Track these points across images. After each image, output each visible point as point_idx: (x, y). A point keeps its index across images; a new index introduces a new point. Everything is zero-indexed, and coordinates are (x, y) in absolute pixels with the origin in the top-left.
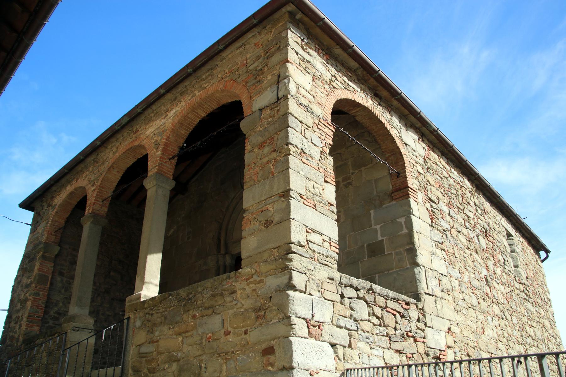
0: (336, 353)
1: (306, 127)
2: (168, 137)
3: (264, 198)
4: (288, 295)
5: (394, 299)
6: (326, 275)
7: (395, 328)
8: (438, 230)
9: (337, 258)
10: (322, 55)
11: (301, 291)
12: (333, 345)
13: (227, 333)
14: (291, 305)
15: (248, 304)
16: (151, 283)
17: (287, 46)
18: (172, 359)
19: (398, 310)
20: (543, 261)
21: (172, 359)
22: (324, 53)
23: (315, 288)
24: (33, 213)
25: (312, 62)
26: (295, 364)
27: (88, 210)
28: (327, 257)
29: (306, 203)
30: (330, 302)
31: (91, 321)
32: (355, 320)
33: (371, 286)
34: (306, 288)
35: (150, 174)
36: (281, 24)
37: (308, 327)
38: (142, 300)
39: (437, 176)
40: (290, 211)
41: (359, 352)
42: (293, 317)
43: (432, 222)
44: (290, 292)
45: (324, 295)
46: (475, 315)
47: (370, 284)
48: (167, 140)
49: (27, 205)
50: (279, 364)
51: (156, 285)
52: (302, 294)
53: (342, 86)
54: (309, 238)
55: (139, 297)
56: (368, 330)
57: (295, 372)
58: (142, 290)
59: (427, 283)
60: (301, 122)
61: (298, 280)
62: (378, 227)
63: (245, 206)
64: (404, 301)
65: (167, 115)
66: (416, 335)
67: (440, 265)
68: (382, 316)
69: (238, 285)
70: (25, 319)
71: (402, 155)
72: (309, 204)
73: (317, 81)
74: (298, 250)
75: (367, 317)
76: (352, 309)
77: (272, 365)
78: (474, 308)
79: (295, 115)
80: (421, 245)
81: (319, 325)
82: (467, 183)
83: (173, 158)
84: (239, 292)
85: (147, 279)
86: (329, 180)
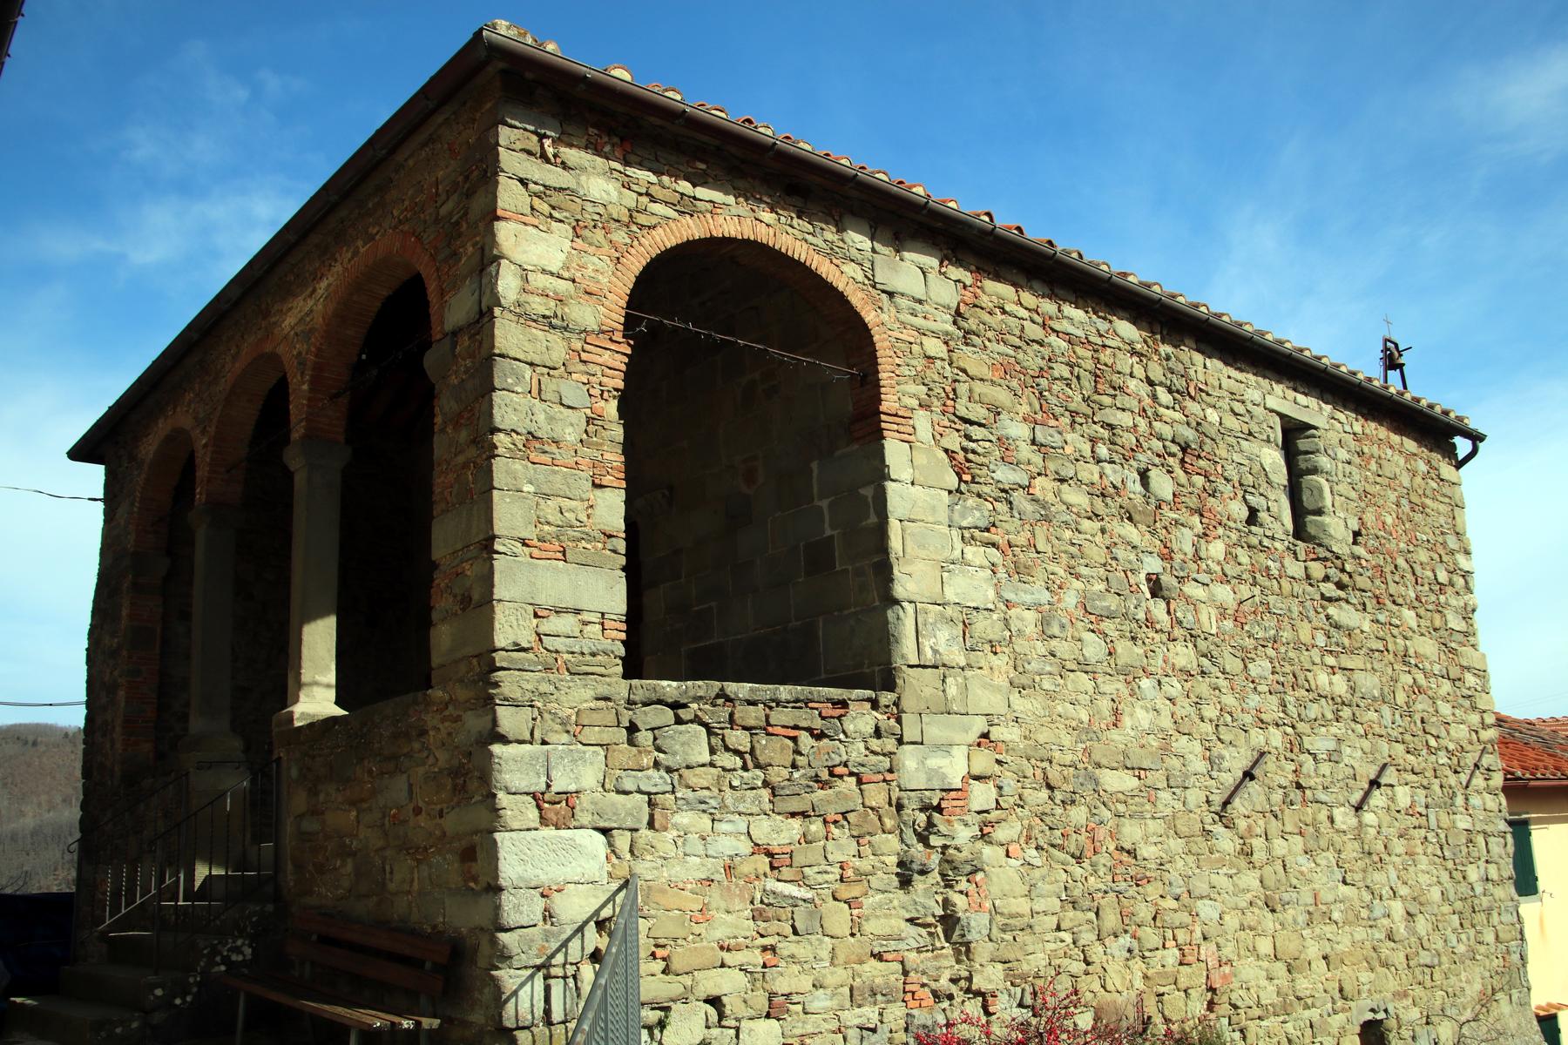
0: (610, 845)
1: (546, 370)
2: (319, 349)
3: (459, 546)
4: (491, 755)
5: (797, 701)
6: (590, 693)
7: (794, 766)
8: (979, 496)
9: (622, 651)
10: (607, 149)
11: (521, 742)
12: (605, 832)
13: (418, 811)
14: (495, 774)
15: (442, 757)
16: (316, 683)
17: (496, 174)
18: (345, 852)
19: (804, 724)
20: (1459, 465)
21: (345, 852)
22: (616, 140)
23: (558, 727)
24: (102, 468)
25: (573, 185)
26: (502, 882)
27: (200, 495)
28: (593, 655)
29: (536, 552)
30: (598, 749)
31: (237, 744)
32: (669, 770)
33: (722, 689)
34: (532, 734)
35: (295, 436)
36: (488, 105)
37: (539, 807)
38: (297, 724)
39: (1002, 348)
40: (492, 586)
41: (675, 833)
42: (501, 795)
43: (961, 480)
44: (497, 749)
45: (580, 738)
46: (1090, 686)
47: (717, 684)
48: (316, 356)
49: (81, 452)
50: (483, 880)
51: (328, 686)
52: (527, 747)
53: (671, 213)
54: (541, 630)
55: (290, 718)
56: (705, 784)
57: (504, 896)
58: (296, 701)
59: (918, 635)
60: (531, 364)
61: (507, 719)
62: (825, 504)
63: (437, 554)
64: (829, 700)
65: (314, 291)
66: (862, 769)
67: (973, 585)
68: (752, 748)
69: (431, 720)
70: (118, 729)
71: (868, 331)
72: (544, 555)
73: (586, 233)
74: (512, 660)
75: (706, 758)
76: (659, 749)
77: (475, 880)
78: (1089, 668)
79: (512, 354)
80: (908, 550)
81: (568, 797)
82: (1126, 329)
83: (336, 396)
84: (432, 733)
85: (306, 676)
86: (607, 480)
